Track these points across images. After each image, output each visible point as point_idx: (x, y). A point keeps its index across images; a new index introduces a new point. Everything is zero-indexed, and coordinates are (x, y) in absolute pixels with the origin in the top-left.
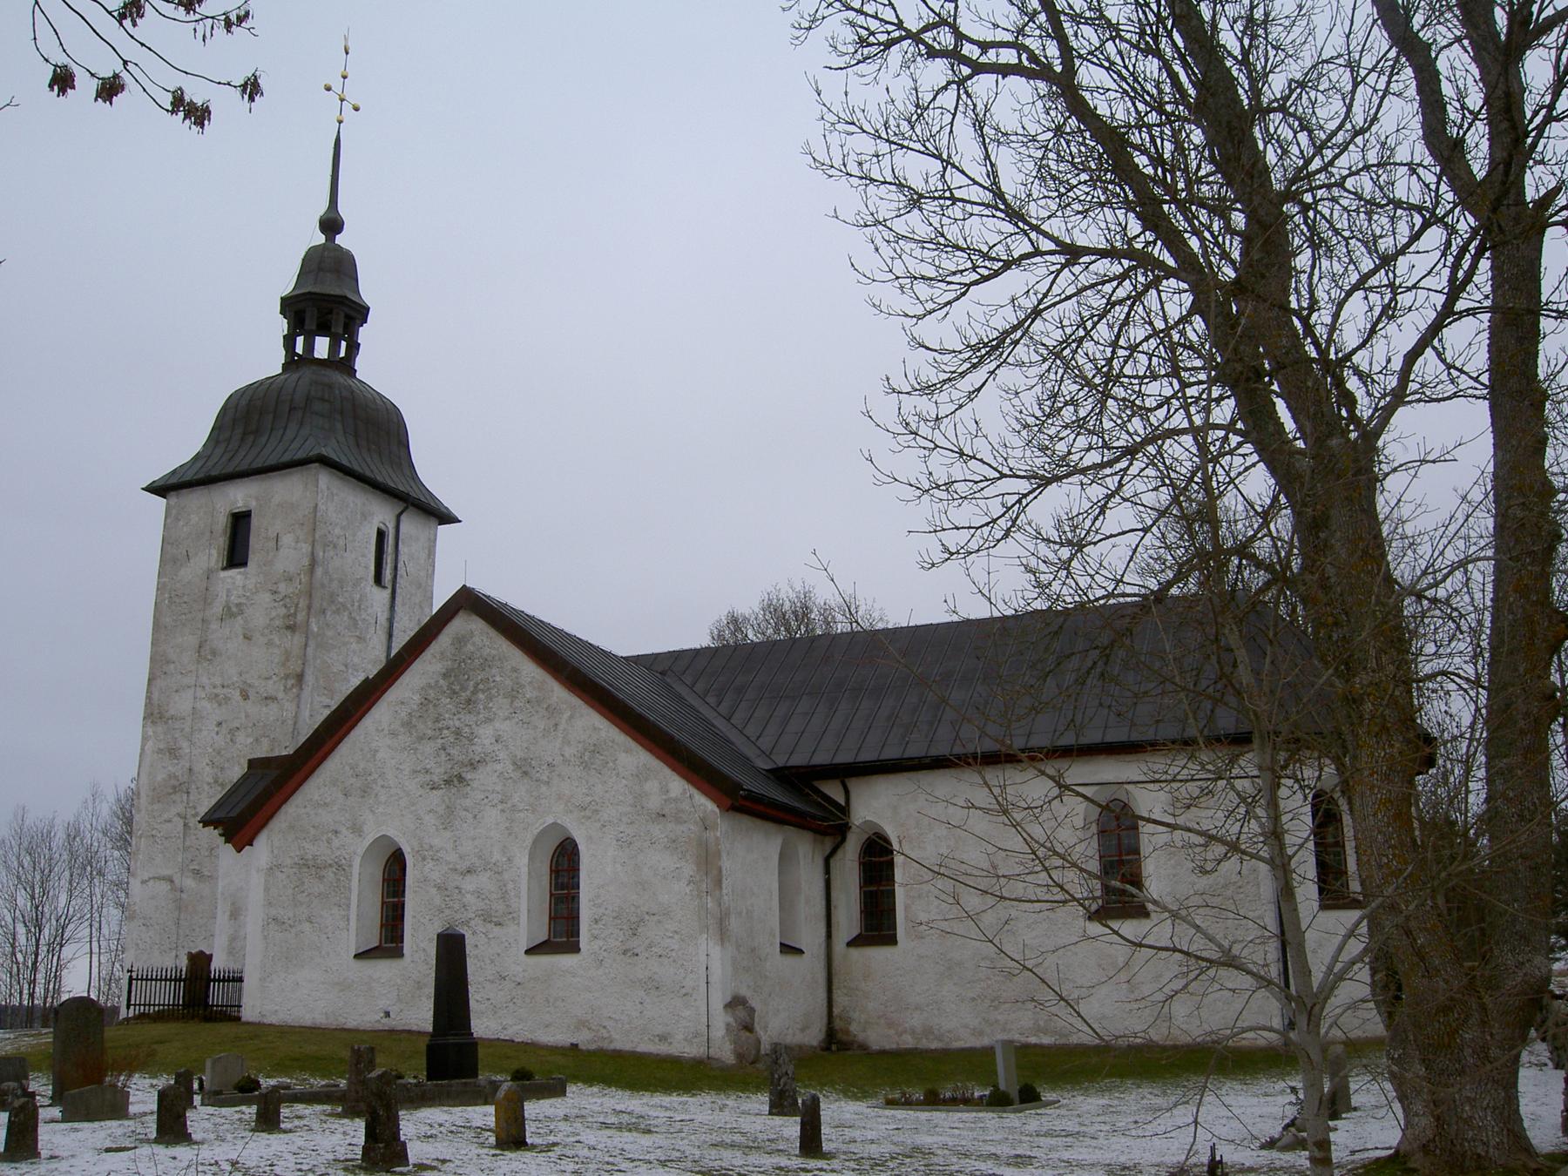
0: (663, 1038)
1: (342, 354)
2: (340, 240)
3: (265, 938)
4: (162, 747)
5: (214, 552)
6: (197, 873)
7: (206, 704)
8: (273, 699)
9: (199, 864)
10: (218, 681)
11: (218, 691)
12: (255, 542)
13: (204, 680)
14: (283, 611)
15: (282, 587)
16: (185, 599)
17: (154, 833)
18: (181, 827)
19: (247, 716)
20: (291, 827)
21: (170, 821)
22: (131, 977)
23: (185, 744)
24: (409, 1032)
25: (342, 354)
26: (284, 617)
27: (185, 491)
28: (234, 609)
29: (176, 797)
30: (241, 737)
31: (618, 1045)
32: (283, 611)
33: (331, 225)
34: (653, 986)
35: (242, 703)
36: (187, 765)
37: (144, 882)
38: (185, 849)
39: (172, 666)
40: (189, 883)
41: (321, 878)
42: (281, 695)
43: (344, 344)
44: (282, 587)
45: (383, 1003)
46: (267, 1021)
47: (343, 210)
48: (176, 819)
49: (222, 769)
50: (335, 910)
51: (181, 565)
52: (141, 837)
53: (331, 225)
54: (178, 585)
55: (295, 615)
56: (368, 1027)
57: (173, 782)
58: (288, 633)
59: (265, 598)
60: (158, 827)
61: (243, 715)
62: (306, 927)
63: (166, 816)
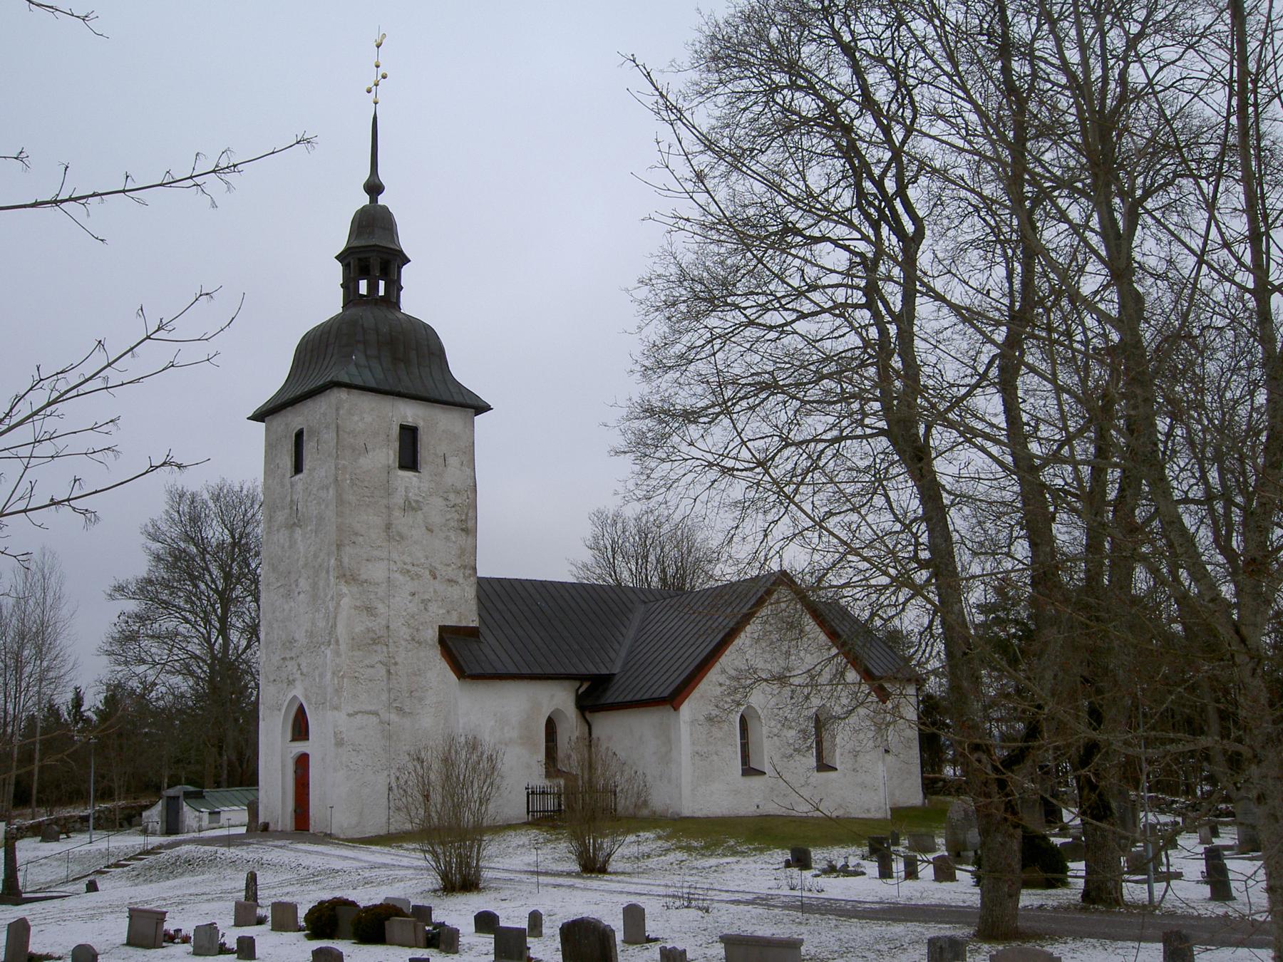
0: (868, 810)
1: (382, 293)
2: (382, 200)
3: (693, 764)
4: (358, 604)
5: (391, 453)
6: (400, 710)
7: (397, 575)
8: (456, 582)
9: (400, 703)
10: (408, 560)
11: (409, 567)
12: (424, 454)
13: (395, 556)
14: (456, 516)
15: (452, 496)
16: (366, 484)
17: (356, 674)
18: (383, 672)
19: (435, 591)
20: (702, 697)
21: (372, 667)
22: (528, 793)
23: (380, 606)
24: (769, 815)
25: (382, 293)
26: (458, 521)
27: (356, 391)
28: (414, 504)
29: (378, 648)
30: (433, 607)
31: (853, 816)
32: (456, 516)
33: (374, 188)
34: (864, 786)
35: (432, 581)
36: (384, 623)
37: (349, 715)
38: (390, 690)
39: (361, 539)
40: (394, 717)
41: (721, 728)
42: (461, 580)
43: (382, 284)
44: (452, 496)
45: (756, 801)
46: (696, 815)
47: (383, 176)
48: (379, 665)
49: (418, 630)
50: (729, 748)
51: (360, 454)
52: (343, 677)
53: (374, 188)
54: (358, 471)
55: (466, 521)
56: (750, 814)
57: (371, 635)
58: (463, 534)
59: (438, 502)
60: (361, 670)
61: (431, 590)
62: (715, 757)
63: (367, 662)
